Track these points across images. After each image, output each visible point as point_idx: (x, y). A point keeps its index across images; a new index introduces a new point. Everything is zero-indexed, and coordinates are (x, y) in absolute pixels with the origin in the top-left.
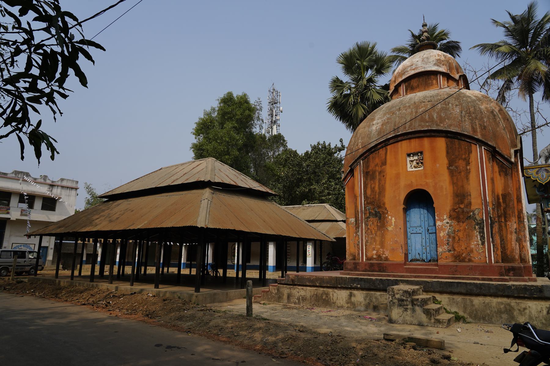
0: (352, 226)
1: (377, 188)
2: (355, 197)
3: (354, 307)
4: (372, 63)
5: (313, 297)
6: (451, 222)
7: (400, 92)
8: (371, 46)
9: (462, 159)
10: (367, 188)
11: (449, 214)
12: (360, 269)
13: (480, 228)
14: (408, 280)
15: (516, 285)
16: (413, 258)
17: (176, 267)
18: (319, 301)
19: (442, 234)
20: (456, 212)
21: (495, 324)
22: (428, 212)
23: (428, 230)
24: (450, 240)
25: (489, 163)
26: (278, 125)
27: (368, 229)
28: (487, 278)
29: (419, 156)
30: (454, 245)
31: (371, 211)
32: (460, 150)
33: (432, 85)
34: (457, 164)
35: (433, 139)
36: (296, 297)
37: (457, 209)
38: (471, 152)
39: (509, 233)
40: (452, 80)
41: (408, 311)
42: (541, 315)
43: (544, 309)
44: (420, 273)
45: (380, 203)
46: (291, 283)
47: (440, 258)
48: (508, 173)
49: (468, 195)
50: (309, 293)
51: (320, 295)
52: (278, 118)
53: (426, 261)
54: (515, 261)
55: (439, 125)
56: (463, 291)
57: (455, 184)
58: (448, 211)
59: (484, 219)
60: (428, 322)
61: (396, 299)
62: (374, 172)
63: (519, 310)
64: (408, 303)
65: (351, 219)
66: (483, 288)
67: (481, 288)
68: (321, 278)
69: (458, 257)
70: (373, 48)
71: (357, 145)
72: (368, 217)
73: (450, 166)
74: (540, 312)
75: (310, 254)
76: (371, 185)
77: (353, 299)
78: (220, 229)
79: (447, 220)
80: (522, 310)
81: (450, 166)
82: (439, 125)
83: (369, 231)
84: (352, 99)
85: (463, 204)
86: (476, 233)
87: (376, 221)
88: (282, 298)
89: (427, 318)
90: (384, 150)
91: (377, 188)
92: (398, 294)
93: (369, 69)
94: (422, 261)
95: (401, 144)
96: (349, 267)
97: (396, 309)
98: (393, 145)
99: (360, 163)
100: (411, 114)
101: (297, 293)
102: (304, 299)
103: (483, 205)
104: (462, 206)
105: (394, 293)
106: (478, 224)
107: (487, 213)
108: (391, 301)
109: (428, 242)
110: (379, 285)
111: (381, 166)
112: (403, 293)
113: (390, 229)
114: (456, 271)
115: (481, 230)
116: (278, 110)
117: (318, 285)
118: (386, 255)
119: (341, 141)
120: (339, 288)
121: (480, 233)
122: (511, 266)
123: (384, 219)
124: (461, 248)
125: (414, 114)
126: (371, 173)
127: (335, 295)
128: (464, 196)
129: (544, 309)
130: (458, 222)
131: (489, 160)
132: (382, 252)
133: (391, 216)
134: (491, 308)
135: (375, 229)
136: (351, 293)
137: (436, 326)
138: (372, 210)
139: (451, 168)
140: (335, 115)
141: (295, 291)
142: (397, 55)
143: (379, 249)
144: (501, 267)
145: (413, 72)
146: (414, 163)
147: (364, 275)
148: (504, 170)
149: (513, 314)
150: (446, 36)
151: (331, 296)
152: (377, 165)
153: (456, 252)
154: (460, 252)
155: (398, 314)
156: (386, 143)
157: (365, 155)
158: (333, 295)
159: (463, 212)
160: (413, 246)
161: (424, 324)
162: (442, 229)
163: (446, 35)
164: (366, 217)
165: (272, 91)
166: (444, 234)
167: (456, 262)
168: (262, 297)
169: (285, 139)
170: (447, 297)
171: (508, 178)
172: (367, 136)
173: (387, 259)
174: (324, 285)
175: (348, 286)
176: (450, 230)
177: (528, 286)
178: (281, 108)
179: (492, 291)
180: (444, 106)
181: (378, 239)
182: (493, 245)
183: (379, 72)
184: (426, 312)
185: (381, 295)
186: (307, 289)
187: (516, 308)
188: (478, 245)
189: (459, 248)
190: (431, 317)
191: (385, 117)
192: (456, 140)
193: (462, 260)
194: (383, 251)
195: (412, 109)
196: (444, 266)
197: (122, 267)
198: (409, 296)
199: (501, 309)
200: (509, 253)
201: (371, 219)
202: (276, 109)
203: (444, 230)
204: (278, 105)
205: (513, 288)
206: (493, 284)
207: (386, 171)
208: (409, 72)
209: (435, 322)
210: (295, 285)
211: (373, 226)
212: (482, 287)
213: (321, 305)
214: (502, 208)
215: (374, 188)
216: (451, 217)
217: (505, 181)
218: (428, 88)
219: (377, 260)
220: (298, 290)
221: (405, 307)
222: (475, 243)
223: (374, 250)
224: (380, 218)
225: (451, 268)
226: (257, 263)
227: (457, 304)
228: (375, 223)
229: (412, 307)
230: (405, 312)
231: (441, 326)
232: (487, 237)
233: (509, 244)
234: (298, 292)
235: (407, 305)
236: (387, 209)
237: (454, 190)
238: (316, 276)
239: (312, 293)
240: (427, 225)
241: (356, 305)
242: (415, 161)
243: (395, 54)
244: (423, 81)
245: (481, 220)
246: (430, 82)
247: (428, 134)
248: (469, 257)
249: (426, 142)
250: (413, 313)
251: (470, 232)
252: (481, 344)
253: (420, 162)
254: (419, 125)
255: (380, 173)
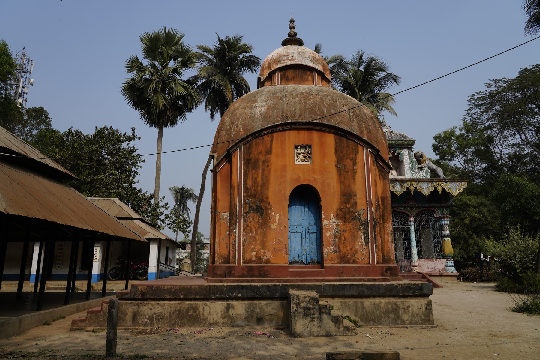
0: (224, 223)
1: (259, 179)
2: (231, 187)
3: (231, 323)
4: (176, 54)
5: (175, 314)
6: (337, 221)
7: (274, 79)
8: (178, 35)
9: (349, 158)
10: (247, 178)
11: (336, 213)
12: (236, 274)
13: (364, 229)
14: (299, 285)
15: (402, 284)
16: (292, 260)
17: (17, 281)
18: (182, 319)
19: (328, 234)
20: (343, 211)
21: (383, 325)
22: (309, 210)
23: (309, 229)
24: (336, 240)
25: (374, 165)
26: (25, 99)
27: (247, 226)
28: (372, 279)
29: (306, 149)
30: (340, 246)
31: (251, 205)
32: (348, 149)
33: (308, 81)
34: (344, 163)
35: (323, 133)
36: (147, 317)
37: (344, 208)
38: (358, 153)
39: (386, 234)
40: (325, 81)
41: (315, 321)
42: (421, 311)
43: (423, 306)
44: (306, 276)
45: (263, 197)
46: (140, 297)
47: (326, 260)
48: (386, 177)
49: (354, 195)
50: (167, 309)
51: (185, 311)
52: (26, 90)
53: (305, 263)
54: (391, 261)
55: (329, 120)
56: (355, 293)
57: (342, 182)
58: (335, 210)
59: (369, 220)
60: (337, 332)
61: (302, 308)
62: (257, 160)
63: (404, 309)
64: (315, 311)
65: (223, 214)
66: (374, 289)
67: (371, 290)
68: (188, 288)
69: (343, 258)
70: (180, 38)
71: (237, 127)
72: (247, 212)
73: (338, 164)
74: (421, 308)
75: (98, 259)
76: (253, 174)
77: (231, 312)
78: (26, 217)
79: (334, 220)
80: (406, 308)
81: (338, 164)
82: (329, 120)
83: (248, 229)
84: (153, 86)
85: (350, 204)
86: (361, 234)
87: (257, 218)
88: (124, 320)
89: (335, 326)
90: (269, 137)
91: (259, 179)
92: (303, 301)
93: (172, 60)
94: (301, 263)
95: (289, 134)
96: (219, 272)
97: (301, 319)
98: (279, 133)
99: (241, 149)
100: (300, 103)
101: (149, 310)
102: (160, 318)
103: (368, 206)
104: (349, 206)
105: (299, 301)
106: (362, 225)
107: (371, 214)
108: (296, 311)
109: (308, 242)
110: (265, 293)
111: (265, 155)
112: (310, 300)
113: (273, 226)
114: (342, 273)
115: (365, 231)
116: (27, 81)
117: (182, 297)
118: (269, 257)
119: (133, 129)
120: (212, 299)
121: (364, 233)
122: (389, 266)
123: (267, 216)
124: (346, 249)
125: (304, 104)
126: (253, 161)
127: (207, 308)
128: (350, 195)
129: (423, 306)
130: (345, 222)
131: (373, 162)
132: (262, 254)
133: (275, 212)
134: (380, 309)
135: (255, 226)
136: (229, 305)
137: (345, 335)
138: (252, 204)
139: (339, 166)
140: (128, 99)
141: (146, 308)
142: (202, 53)
143: (259, 250)
144: (383, 267)
145: (289, 63)
146: (301, 156)
147: (242, 281)
148: (383, 174)
149: (398, 313)
150: (250, 49)
151: (201, 310)
152: (260, 153)
153: (341, 253)
154: (345, 253)
155: (303, 326)
156: (273, 129)
157: (247, 140)
158: (204, 308)
159: (349, 211)
160: (293, 247)
161: (333, 334)
162: (328, 229)
163: (249, 48)
164: (245, 211)
165: (20, 56)
166: (331, 234)
167: (342, 263)
168: (87, 321)
169: (49, 116)
170: (340, 301)
171: (386, 182)
172: (249, 118)
173: (268, 261)
174: (192, 297)
175: (225, 296)
176: (336, 230)
177: (412, 284)
178: (32, 80)
179: (381, 292)
180: (332, 102)
181: (258, 238)
182: (376, 246)
183: (185, 64)
184: (334, 320)
185: (267, 305)
186: (165, 304)
187: (401, 306)
188: (362, 245)
189: (345, 249)
190: (340, 325)
191: (270, 101)
192: (345, 139)
193: (347, 261)
194: (264, 252)
195: (300, 99)
196: (330, 268)
197: (38, 291)
198: (317, 304)
199: (388, 309)
200: (386, 254)
201: (252, 214)
202: (24, 80)
203: (331, 230)
204: (28, 75)
205: (399, 287)
206: (382, 285)
207: (271, 161)
208: (286, 62)
209: (343, 331)
210: (147, 299)
211: (253, 223)
212: (373, 288)
213: (185, 324)
214: (381, 210)
215: (256, 178)
216: (337, 217)
217: (384, 185)
218: (303, 82)
219: (256, 263)
220: (150, 306)
221: (311, 316)
222: (360, 243)
223: (254, 251)
224: (262, 214)
225: (337, 270)
226: (66, 271)
227: (349, 308)
228: (256, 220)
229: (319, 316)
230: (311, 323)
231: (350, 334)
232: (371, 237)
233: (386, 245)
234: (151, 309)
235: (314, 314)
236: (271, 204)
237: (341, 189)
238: (180, 286)
239: (173, 309)
240: (308, 225)
241: (235, 319)
242: (302, 154)
243: (200, 51)
244: (299, 74)
245: (365, 221)
246: (306, 77)
247: (319, 128)
248: (354, 258)
249: (315, 135)
250: (320, 323)
251: (355, 233)
252: (411, 349)
253: (308, 156)
254: (310, 117)
255: (264, 162)
